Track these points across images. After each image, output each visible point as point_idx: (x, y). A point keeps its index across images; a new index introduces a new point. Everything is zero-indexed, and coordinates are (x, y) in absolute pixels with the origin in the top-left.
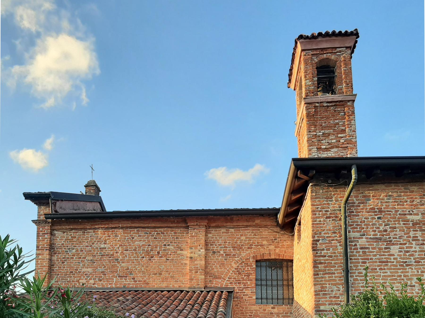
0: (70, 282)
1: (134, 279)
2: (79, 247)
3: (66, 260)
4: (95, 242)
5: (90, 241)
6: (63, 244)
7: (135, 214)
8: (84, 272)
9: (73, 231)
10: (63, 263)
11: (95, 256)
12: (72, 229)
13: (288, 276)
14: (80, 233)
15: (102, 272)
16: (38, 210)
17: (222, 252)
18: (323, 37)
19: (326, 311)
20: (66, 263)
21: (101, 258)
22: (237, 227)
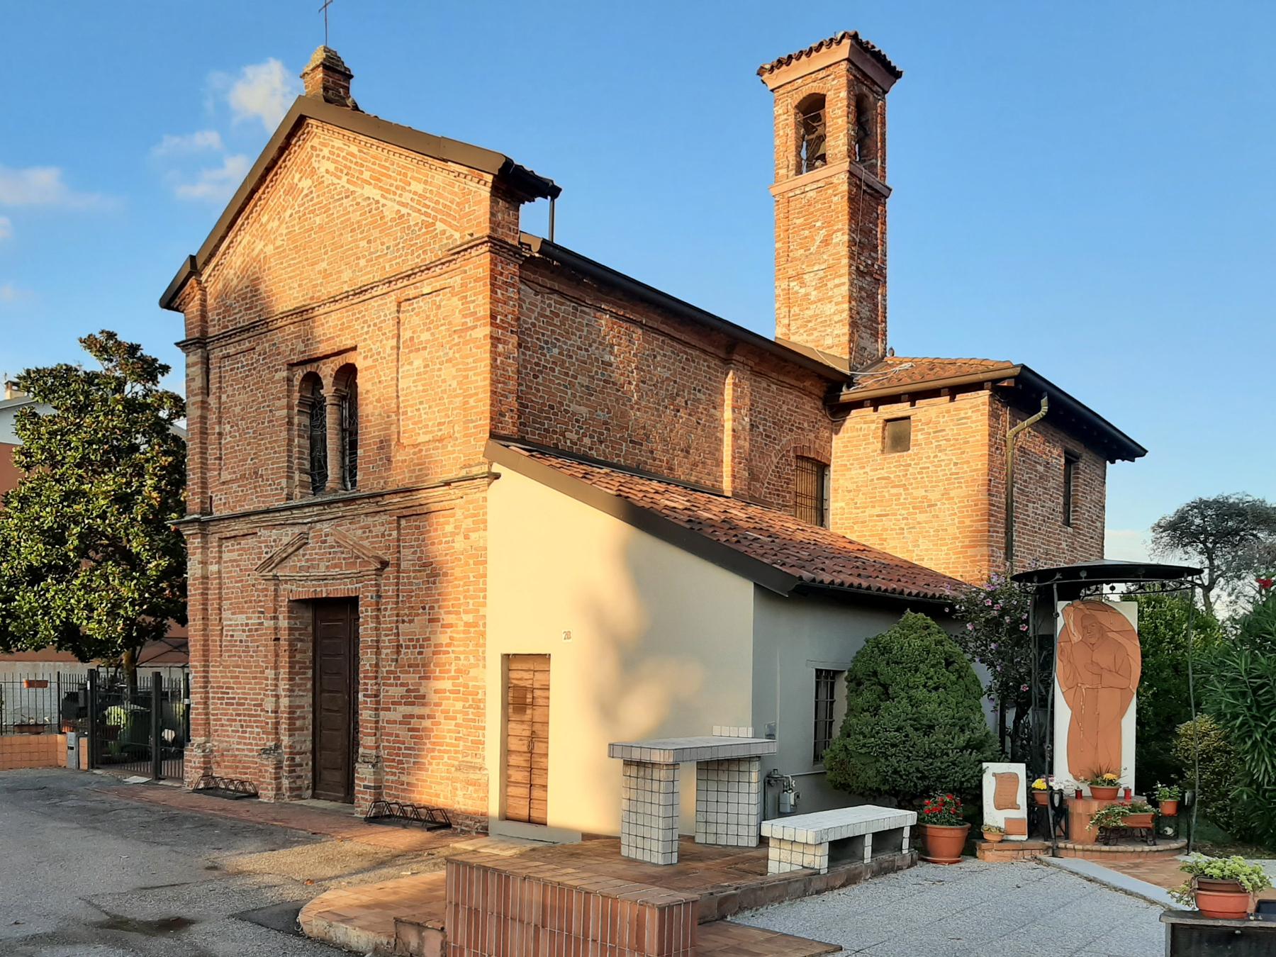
0: (546, 430)
1: (652, 452)
2: (565, 343)
3: (541, 372)
4: (594, 341)
5: (587, 338)
6: (534, 325)
7: (603, 273)
8: (574, 414)
9: (555, 297)
10: (536, 377)
11: (592, 377)
12: (553, 291)
13: (395, 492)
14: (569, 307)
15: (605, 423)
16: (492, 207)
17: (761, 429)
18: (1144, 841)
19: (405, 704)
20: (540, 380)
21: (604, 387)
22: (781, 384)
